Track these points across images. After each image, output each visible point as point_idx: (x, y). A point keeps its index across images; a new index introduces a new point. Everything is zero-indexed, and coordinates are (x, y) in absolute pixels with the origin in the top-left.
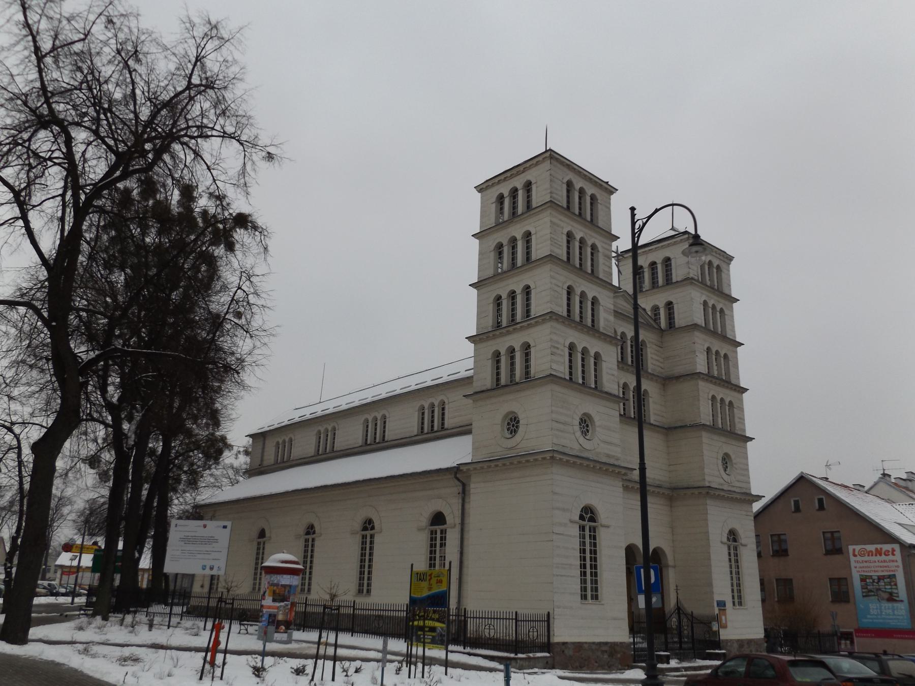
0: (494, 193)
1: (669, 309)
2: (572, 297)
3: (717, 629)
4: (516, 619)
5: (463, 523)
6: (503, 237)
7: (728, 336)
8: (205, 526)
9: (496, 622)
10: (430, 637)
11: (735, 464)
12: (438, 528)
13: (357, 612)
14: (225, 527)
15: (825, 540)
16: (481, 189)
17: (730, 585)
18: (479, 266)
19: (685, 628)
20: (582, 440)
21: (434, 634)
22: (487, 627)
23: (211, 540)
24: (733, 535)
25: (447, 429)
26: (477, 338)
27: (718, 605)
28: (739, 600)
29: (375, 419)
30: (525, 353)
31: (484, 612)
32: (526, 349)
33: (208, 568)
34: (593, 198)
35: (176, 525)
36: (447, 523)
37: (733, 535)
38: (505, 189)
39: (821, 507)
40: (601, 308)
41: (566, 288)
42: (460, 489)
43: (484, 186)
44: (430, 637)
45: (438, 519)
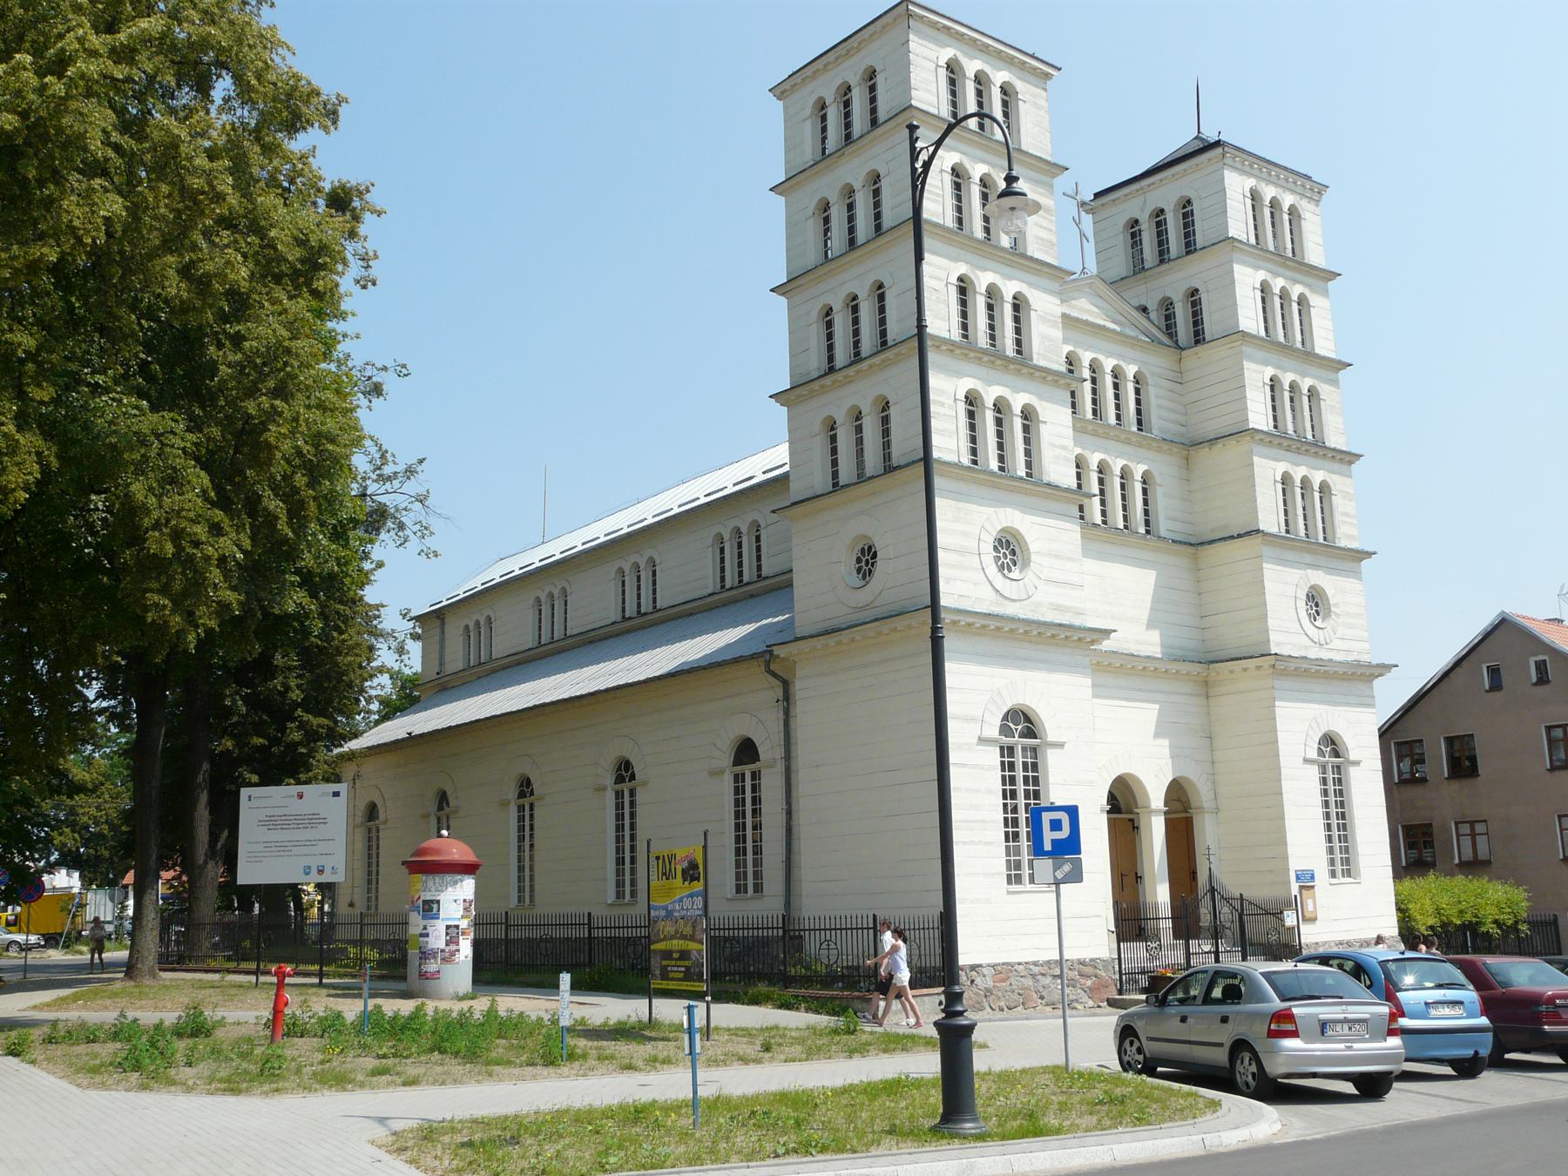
0: (806, 99)
1: (1194, 304)
2: (969, 299)
3: (1295, 923)
4: (506, 923)
5: (788, 757)
6: (828, 186)
7: (1318, 351)
8: (301, 796)
9: (839, 936)
10: (683, 969)
11: (1336, 605)
12: (747, 770)
13: (595, 933)
14: (336, 794)
15: (1551, 741)
16: (782, 93)
17: (535, 827)
18: (788, 250)
19: (1228, 925)
20: (999, 581)
21: (687, 963)
22: (824, 946)
23: (315, 820)
24: (1331, 743)
25: (767, 578)
26: (792, 395)
27: (1298, 878)
28: (1343, 860)
29: (637, 567)
30: (882, 418)
31: (833, 918)
32: (884, 410)
33: (314, 871)
34: (1005, 90)
35: (250, 797)
36: (762, 757)
37: (1331, 743)
38: (827, 88)
39: (1543, 679)
40: (1033, 314)
41: (955, 282)
42: (779, 693)
43: (787, 86)
44: (683, 969)
45: (746, 751)
